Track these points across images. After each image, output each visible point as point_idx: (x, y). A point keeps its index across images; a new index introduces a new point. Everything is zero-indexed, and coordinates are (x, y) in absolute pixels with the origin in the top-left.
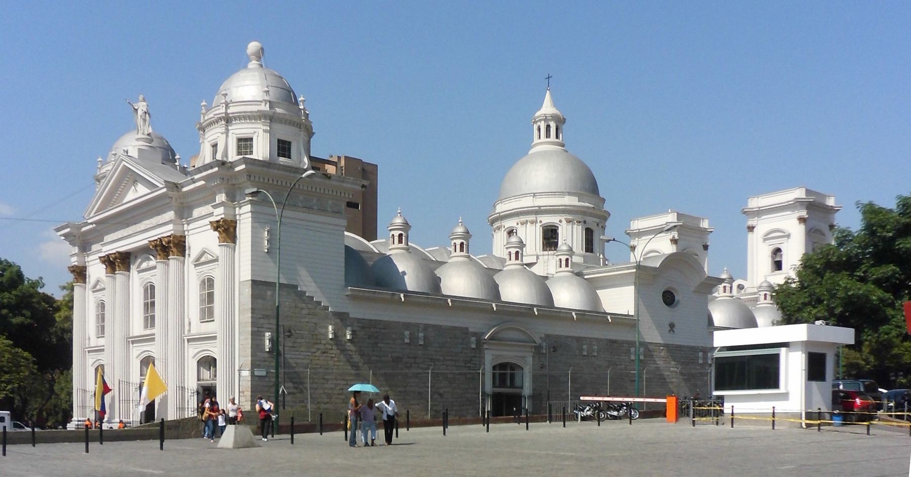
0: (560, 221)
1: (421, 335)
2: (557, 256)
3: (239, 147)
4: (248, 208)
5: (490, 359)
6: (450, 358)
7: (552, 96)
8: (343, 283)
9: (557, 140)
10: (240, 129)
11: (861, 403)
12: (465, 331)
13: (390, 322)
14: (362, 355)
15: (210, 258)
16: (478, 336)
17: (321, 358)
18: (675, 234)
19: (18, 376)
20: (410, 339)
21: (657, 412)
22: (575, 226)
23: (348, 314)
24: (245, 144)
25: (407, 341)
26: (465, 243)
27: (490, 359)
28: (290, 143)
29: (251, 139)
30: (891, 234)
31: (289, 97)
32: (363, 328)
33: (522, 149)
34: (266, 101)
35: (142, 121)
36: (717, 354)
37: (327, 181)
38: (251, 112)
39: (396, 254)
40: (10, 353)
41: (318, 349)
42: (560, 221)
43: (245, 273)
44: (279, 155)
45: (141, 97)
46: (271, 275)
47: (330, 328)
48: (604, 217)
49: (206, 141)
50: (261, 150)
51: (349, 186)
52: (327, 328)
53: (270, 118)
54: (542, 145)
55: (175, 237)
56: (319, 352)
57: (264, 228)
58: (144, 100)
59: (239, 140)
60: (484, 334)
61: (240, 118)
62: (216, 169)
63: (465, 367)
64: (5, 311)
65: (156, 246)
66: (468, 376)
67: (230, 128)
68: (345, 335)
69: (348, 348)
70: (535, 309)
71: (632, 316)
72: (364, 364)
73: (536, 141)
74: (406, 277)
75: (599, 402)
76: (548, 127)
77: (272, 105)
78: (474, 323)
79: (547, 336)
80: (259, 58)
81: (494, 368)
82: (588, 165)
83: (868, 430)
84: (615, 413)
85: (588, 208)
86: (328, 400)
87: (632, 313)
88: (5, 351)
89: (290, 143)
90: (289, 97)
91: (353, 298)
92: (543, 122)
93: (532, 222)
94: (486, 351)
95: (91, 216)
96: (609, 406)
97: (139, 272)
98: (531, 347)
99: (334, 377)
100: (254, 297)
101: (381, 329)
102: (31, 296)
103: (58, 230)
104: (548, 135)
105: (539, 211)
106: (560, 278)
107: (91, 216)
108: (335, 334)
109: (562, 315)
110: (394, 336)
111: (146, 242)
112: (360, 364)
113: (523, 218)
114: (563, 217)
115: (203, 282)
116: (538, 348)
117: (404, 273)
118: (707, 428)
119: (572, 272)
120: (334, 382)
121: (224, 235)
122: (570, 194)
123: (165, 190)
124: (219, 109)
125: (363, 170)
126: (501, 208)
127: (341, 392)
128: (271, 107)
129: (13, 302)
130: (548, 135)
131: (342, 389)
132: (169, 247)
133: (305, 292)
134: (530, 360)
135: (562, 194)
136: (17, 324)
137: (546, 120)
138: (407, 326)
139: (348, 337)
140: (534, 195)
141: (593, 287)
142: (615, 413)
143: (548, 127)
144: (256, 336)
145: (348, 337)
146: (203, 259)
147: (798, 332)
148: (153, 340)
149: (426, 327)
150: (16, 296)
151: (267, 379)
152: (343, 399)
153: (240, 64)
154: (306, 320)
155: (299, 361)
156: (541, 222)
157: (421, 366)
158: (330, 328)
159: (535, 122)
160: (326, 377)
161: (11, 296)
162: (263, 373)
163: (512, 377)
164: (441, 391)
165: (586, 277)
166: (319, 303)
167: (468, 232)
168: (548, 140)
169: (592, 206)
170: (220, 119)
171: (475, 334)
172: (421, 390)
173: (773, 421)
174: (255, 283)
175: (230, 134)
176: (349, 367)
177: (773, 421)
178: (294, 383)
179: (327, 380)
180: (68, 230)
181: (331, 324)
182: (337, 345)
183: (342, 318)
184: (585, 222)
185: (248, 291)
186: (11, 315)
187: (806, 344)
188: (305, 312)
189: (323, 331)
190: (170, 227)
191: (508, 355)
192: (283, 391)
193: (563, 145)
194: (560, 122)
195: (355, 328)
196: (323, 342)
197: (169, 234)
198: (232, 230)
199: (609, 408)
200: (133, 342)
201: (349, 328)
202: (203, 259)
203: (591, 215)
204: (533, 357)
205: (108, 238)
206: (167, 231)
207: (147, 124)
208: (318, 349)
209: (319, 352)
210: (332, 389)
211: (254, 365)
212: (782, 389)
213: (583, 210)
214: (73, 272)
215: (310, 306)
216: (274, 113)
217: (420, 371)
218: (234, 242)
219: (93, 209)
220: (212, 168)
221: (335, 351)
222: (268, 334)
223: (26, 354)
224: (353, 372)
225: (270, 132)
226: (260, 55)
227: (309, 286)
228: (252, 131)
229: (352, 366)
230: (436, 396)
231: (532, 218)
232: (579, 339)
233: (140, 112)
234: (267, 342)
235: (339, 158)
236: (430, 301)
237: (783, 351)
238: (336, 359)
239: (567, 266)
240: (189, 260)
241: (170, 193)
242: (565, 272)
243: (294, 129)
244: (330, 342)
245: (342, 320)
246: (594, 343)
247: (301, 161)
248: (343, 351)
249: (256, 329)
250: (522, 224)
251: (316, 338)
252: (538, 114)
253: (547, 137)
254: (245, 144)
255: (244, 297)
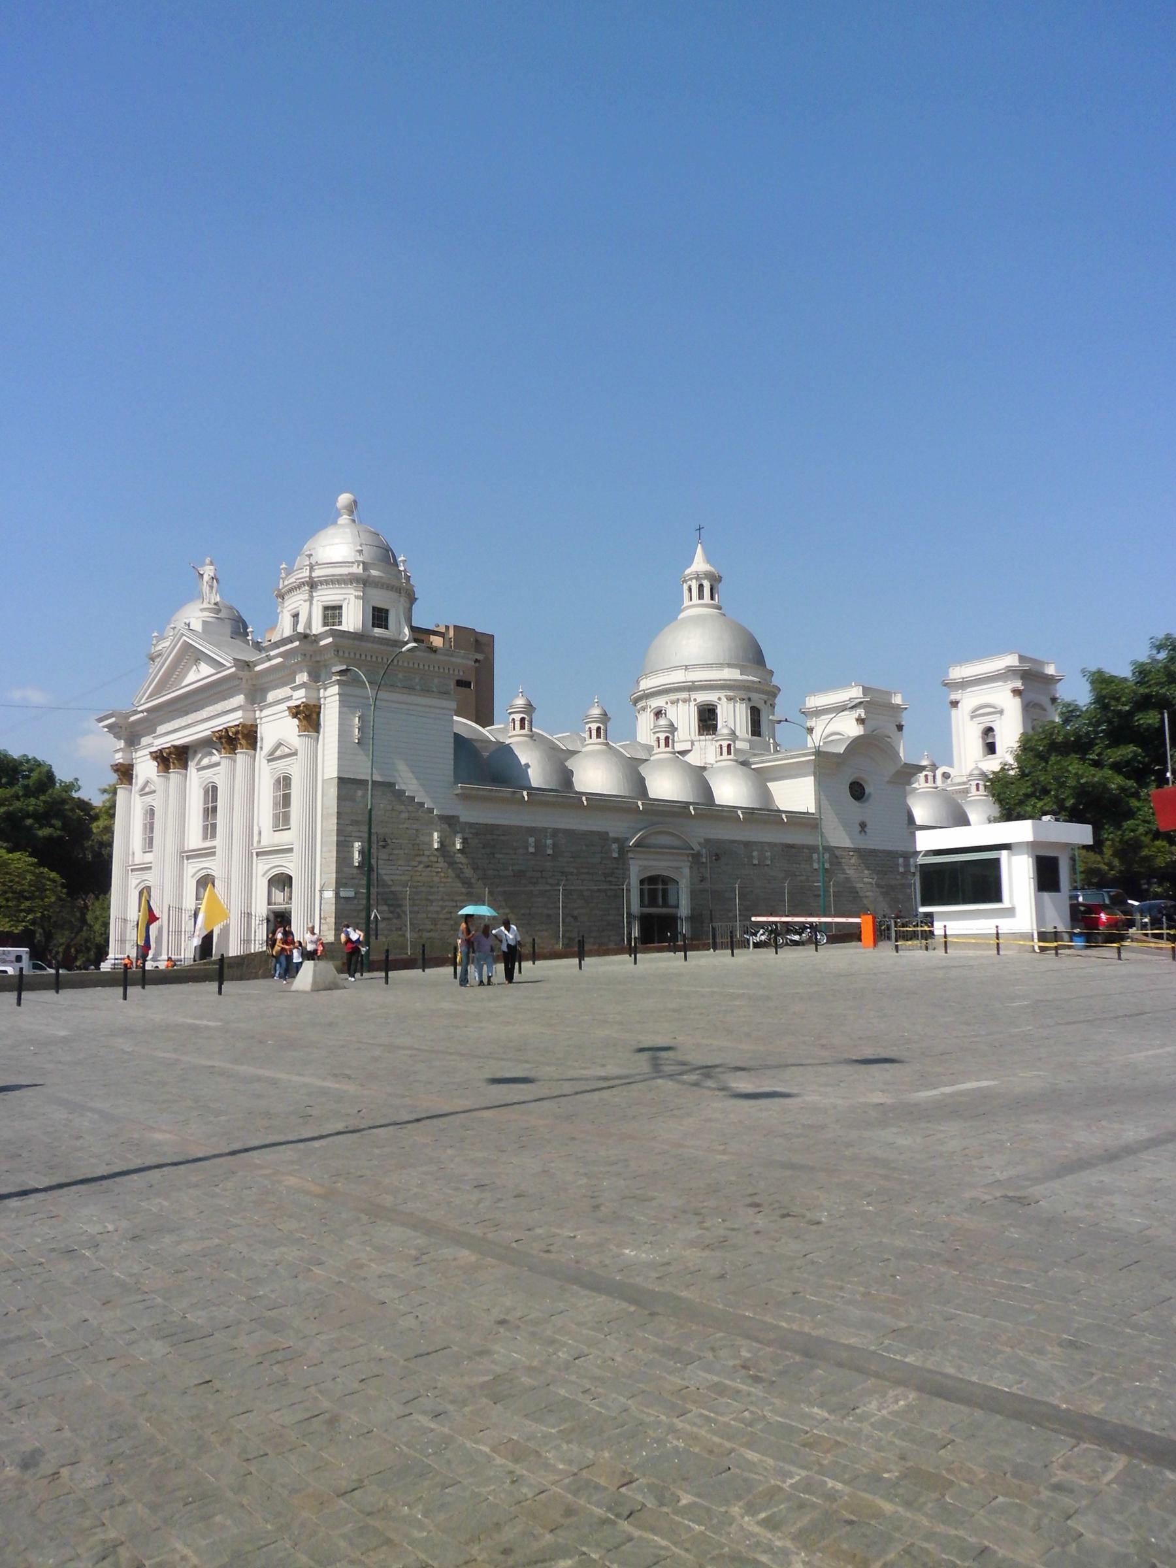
0: (719, 699)
1: (549, 842)
2: (717, 741)
3: (325, 617)
4: (335, 689)
5: (636, 871)
6: (586, 870)
7: (704, 549)
8: (452, 779)
9: (712, 602)
10: (327, 596)
11: (1108, 919)
12: (604, 836)
13: (510, 827)
14: (475, 868)
15: (287, 751)
16: (621, 842)
17: (424, 874)
18: (861, 712)
19: (41, 903)
20: (536, 847)
21: (849, 935)
22: (738, 705)
23: (458, 817)
24: (332, 613)
25: (532, 850)
26: (602, 727)
27: (636, 871)
28: (387, 611)
29: (340, 607)
30: (1127, 708)
31: (387, 557)
32: (477, 834)
33: (669, 613)
34: (358, 562)
35: (208, 588)
36: (921, 860)
37: (433, 656)
38: (341, 575)
39: (517, 743)
40: (33, 873)
41: (420, 862)
42: (719, 699)
43: (330, 768)
44: (374, 626)
45: (208, 560)
46: (363, 770)
47: (436, 835)
48: (773, 693)
49: (285, 610)
50: (353, 619)
51: (459, 661)
52: (432, 836)
53: (364, 582)
54: (694, 608)
55: (244, 726)
56: (422, 866)
57: (354, 714)
58: (211, 563)
59: (326, 608)
60: (628, 839)
61: (327, 582)
62: (297, 643)
63: (606, 881)
64: (29, 822)
65: (220, 738)
66: (609, 893)
67: (314, 594)
68: (454, 845)
69: (458, 861)
70: (691, 808)
71: (813, 814)
72: (478, 880)
73: (687, 603)
74: (530, 771)
75: (775, 923)
76: (701, 587)
77: (366, 566)
78: (614, 826)
79: (707, 841)
80: (351, 512)
81: (642, 882)
82: (751, 631)
83: (1119, 953)
84: (797, 938)
85: (753, 682)
86: (432, 927)
87: (812, 810)
88: (27, 871)
89: (387, 611)
90: (387, 557)
91: (465, 797)
92: (694, 581)
93: (684, 701)
94: (631, 862)
95: (142, 702)
96: (789, 928)
97: (198, 770)
98: (688, 855)
99: (439, 898)
100: (341, 798)
101: (499, 835)
102: (63, 802)
103: (100, 720)
104: (701, 596)
105: (692, 687)
106: (722, 769)
107: (142, 702)
108: (441, 842)
109: (725, 814)
110: (515, 844)
111: (208, 733)
112: (473, 881)
113: (673, 696)
114: (722, 694)
115: (278, 781)
116: (696, 857)
117: (527, 766)
118: (913, 954)
119: (736, 761)
120: (441, 903)
121: (305, 722)
122: (730, 666)
123: (233, 669)
124: (302, 572)
125: (477, 641)
126: (646, 684)
127: (449, 916)
128: (364, 569)
129: (41, 809)
130: (701, 596)
131: (451, 913)
132: (236, 739)
133: (404, 792)
134: (686, 871)
135: (720, 666)
136: (44, 837)
137: (698, 578)
138: (532, 831)
139: (458, 846)
140: (686, 668)
141: (761, 778)
142: (797, 938)
143: (701, 587)
144: (343, 847)
145: (458, 846)
146: (278, 753)
147: (1021, 831)
148: (213, 854)
149: (556, 832)
150: (45, 802)
151: (356, 902)
152: (452, 925)
153: (328, 519)
154: (405, 826)
155: (396, 878)
156: (695, 700)
157: (550, 881)
158: (436, 835)
159: (685, 581)
160: (430, 897)
161: (39, 803)
162: (351, 894)
163: (665, 893)
164: (576, 913)
165: (753, 767)
166: (422, 804)
167: (605, 714)
168: (701, 602)
169: (758, 680)
170: (303, 583)
171: (616, 840)
172: (550, 912)
173: (998, 944)
174: (342, 781)
175: (315, 602)
176: (460, 885)
177: (998, 944)
178: (389, 906)
179: (432, 901)
180: (113, 720)
181: (436, 831)
182: (444, 856)
183: (450, 822)
184: (749, 699)
185: (333, 791)
186: (36, 826)
187: (1032, 846)
188: (404, 815)
189: (426, 839)
190: (239, 714)
191: (660, 866)
192: (376, 917)
193: (719, 608)
194: (715, 580)
195: (466, 835)
196: (427, 853)
197: (237, 723)
198: (314, 716)
199: (789, 932)
200: (188, 858)
201: (459, 835)
202: (278, 753)
203: (757, 691)
204: (691, 867)
205: (161, 729)
206: (234, 719)
207: (214, 591)
208: (420, 862)
209: (422, 866)
210: (437, 912)
211: (340, 884)
212: (1006, 903)
213: (746, 685)
214: (116, 771)
215: (410, 808)
216: (369, 576)
217: (548, 888)
218: (318, 731)
219: (144, 694)
220: (292, 642)
221: (442, 864)
222: (357, 845)
223: (53, 875)
224: (464, 890)
225: (363, 598)
226: (352, 508)
227: (409, 784)
228: (341, 597)
229: (463, 883)
230: (569, 919)
231: (684, 695)
232: (747, 844)
233: (206, 578)
234: (356, 855)
235: (447, 627)
236: (560, 800)
237: (1004, 854)
238: (442, 874)
239: (729, 753)
240: (261, 754)
241: (241, 674)
242: (727, 760)
243: (392, 595)
244: (436, 853)
245: (450, 825)
246: (766, 849)
247: (400, 632)
248: (452, 864)
249: (342, 838)
250: (672, 703)
251: (418, 848)
252: (688, 571)
253: (699, 599)
254: (332, 613)
255: (328, 799)
